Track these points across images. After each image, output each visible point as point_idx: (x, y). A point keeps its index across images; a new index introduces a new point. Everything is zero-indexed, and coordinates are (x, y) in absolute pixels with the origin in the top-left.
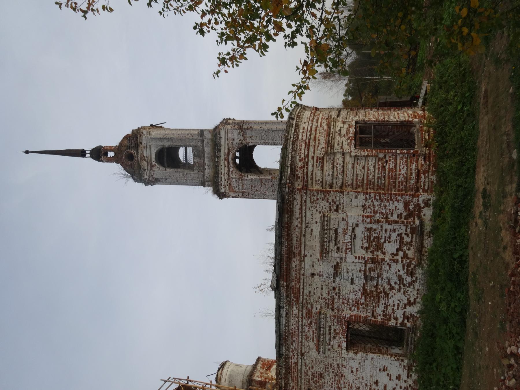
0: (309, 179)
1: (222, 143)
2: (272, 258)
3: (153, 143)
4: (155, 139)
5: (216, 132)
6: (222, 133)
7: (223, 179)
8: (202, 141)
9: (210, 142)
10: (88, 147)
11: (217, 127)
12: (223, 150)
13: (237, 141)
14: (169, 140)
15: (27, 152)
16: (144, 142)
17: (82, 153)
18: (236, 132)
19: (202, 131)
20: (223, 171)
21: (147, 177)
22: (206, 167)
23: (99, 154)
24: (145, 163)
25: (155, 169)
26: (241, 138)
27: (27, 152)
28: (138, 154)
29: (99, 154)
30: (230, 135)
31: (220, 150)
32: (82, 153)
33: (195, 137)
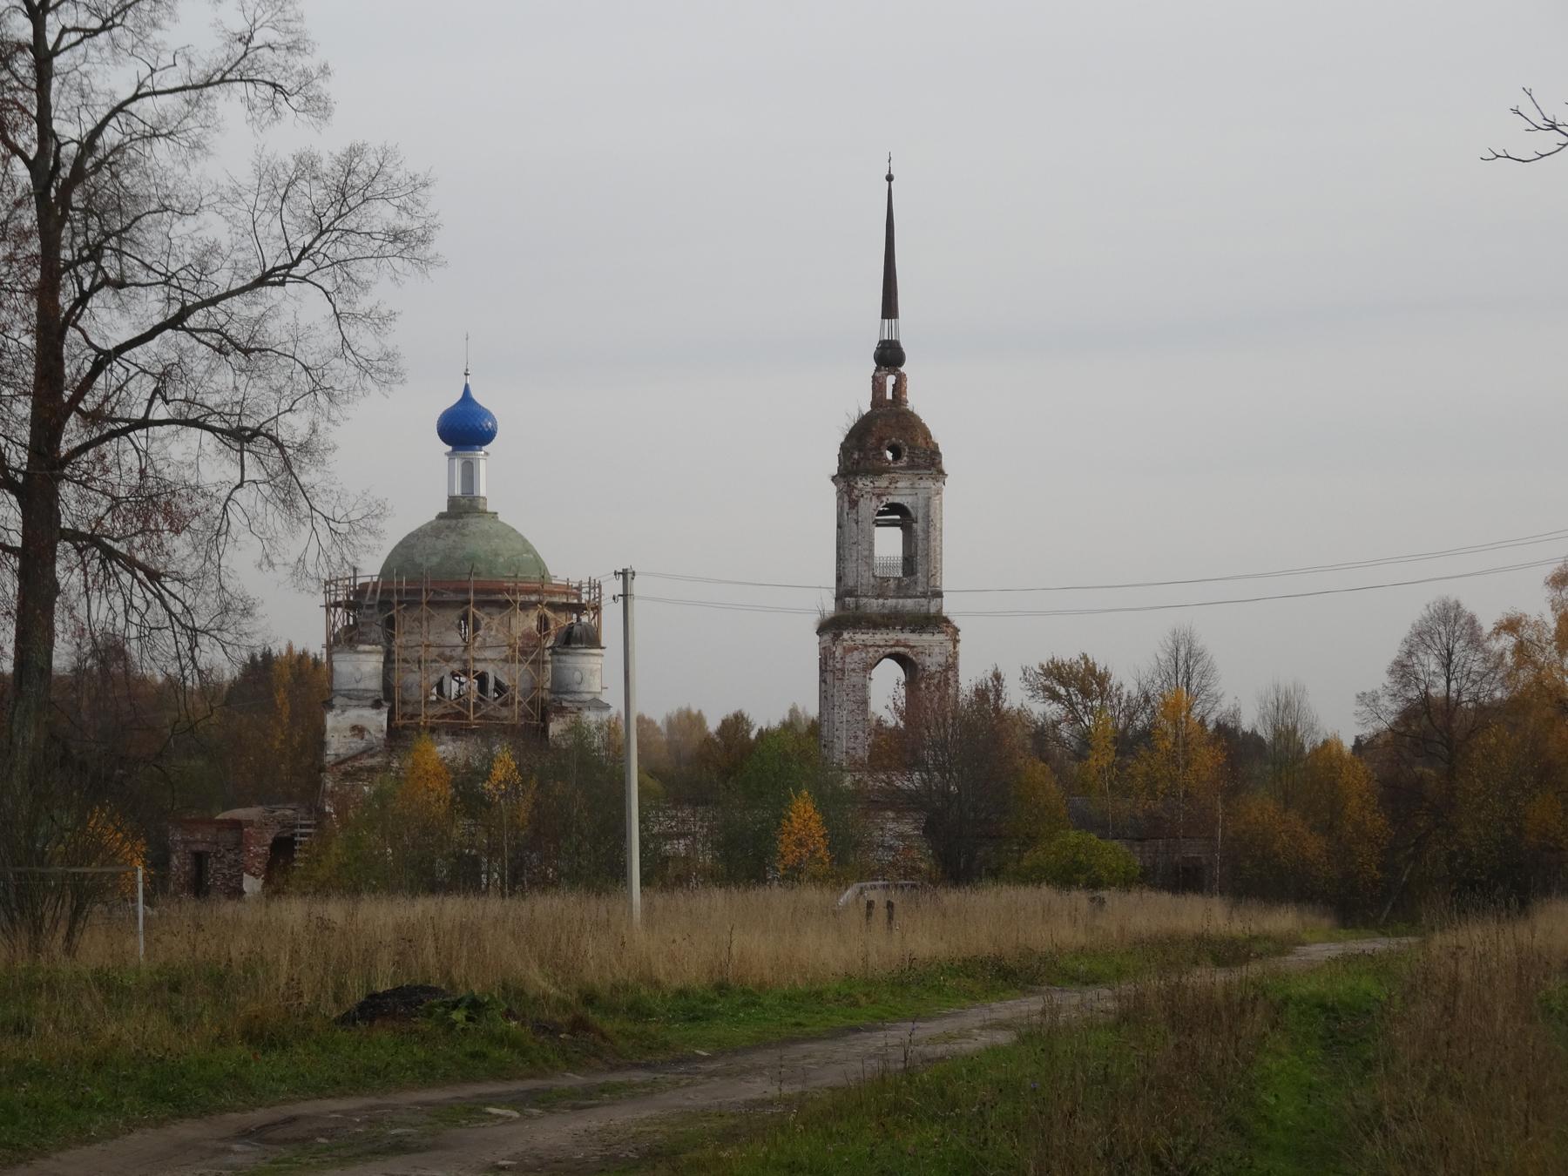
0: (389, 926)
1: (926, 637)
2: (290, 649)
3: (921, 503)
4: (928, 506)
5: (936, 622)
6: (940, 637)
7: (864, 637)
8: (924, 595)
9: (924, 610)
10: (907, 331)
11: (946, 620)
12: (913, 638)
13: (928, 661)
14: (927, 532)
15: (890, 178)
16: (923, 484)
17: (890, 309)
18: (942, 660)
19: (939, 595)
20: (878, 636)
21: (860, 485)
22: (881, 601)
23: (889, 356)
24: (885, 484)
25: (875, 501)
26: (933, 669)
27: (890, 178)
28: (901, 468)
29: (889, 356)
30: (937, 650)
31: (913, 631)
32: (890, 309)
33: (932, 583)
